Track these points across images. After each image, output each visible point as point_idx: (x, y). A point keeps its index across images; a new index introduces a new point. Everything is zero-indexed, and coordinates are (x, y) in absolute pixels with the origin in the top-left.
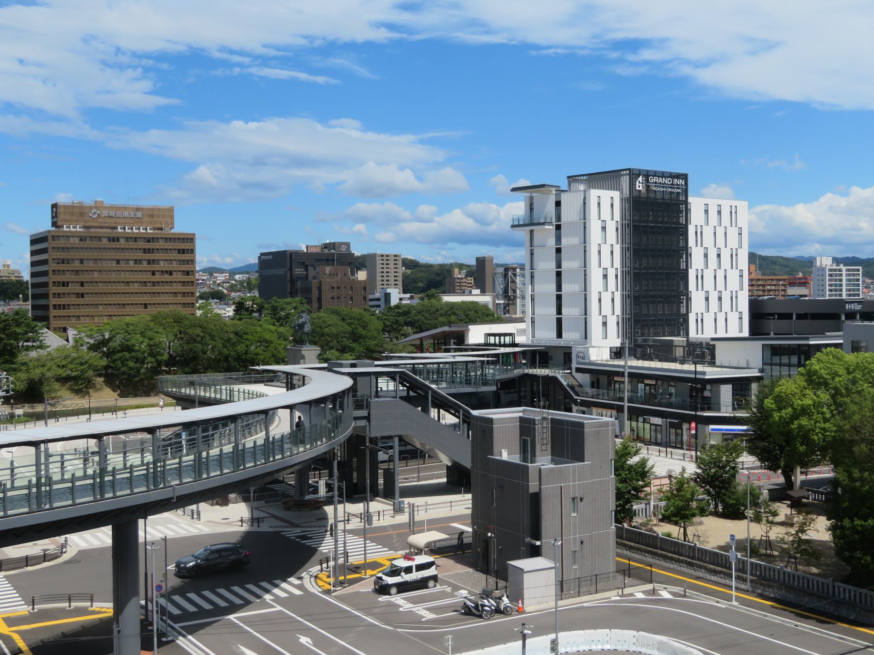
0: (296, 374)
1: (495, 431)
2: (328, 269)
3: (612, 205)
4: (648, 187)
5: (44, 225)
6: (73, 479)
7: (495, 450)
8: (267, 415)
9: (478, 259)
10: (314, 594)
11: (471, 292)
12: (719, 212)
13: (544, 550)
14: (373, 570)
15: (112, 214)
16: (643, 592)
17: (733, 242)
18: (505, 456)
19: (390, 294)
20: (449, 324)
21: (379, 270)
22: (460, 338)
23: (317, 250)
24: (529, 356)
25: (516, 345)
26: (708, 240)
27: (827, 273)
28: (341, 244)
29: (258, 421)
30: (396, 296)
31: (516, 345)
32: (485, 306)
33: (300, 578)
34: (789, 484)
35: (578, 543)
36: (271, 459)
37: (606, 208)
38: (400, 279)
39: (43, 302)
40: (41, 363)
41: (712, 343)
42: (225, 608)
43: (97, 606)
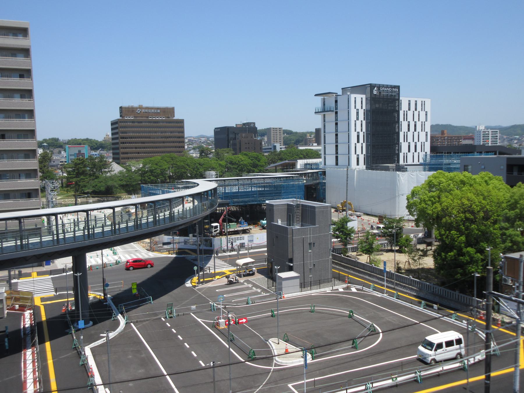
1: (275, 210)
2: (244, 135)
3: (362, 102)
5: (117, 116)
7: (275, 219)
12: (416, 104)
13: (294, 268)
15: (146, 111)
17: (423, 118)
18: (280, 223)
22: (293, 165)
23: (241, 126)
26: (410, 118)
27: (482, 133)
28: (251, 123)
37: (358, 103)
39: (117, 151)
40: (112, 178)
41: (405, 167)
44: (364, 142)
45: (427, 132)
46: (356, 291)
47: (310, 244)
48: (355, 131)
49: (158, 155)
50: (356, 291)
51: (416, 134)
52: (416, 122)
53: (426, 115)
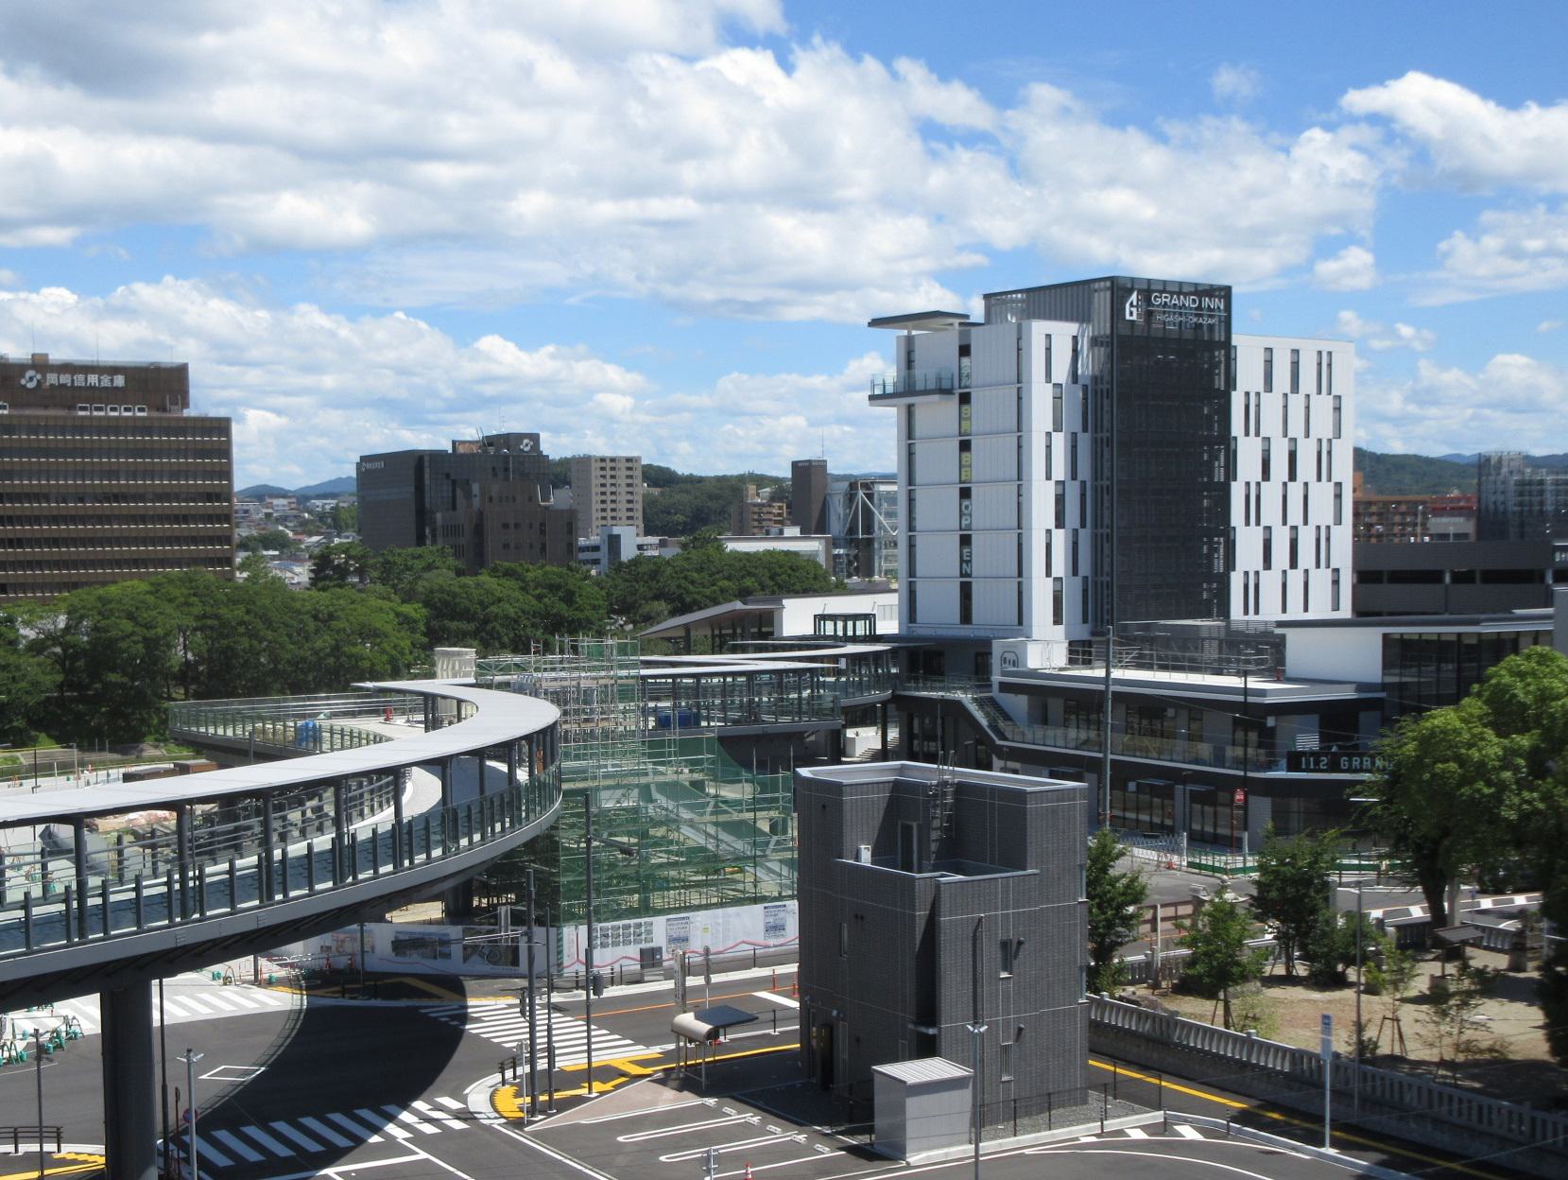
0: (444, 697)
1: (847, 808)
6: (26, 904)
8: (392, 778)
9: (796, 466)
11: (781, 532)
12: (1295, 366)
13: (944, 1044)
14: (604, 1082)
15: (66, 379)
16: (1144, 1128)
17: (1322, 427)
19: (618, 537)
20: (744, 594)
21: (596, 489)
22: (761, 631)
28: (521, 436)
29: (380, 788)
30: (632, 541)
32: (811, 558)
34: (1439, 918)
35: (1013, 1032)
36: (407, 863)
41: (1279, 631)
42: (286, 1159)
43: (68, 1150)
44: (1083, 525)
45: (1339, 485)
46: (1197, 1136)
47: (1005, 945)
48: (1049, 477)
49: (132, 576)
50: (1197, 1136)
51: (1295, 491)
52: (1294, 440)
53: (1338, 409)
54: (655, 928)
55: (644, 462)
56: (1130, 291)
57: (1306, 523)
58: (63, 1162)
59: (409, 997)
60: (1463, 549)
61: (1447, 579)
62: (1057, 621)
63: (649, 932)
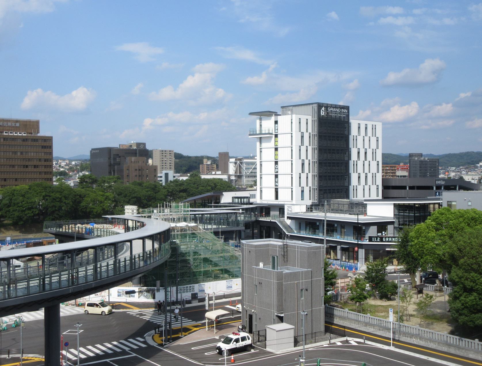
2: (133, 159)
4: (328, 113)
10: (153, 347)
12: (366, 128)
16: (341, 342)
17: (374, 145)
22: (216, 201)
24: (259, 210)
25: (252, 204)
31: (252, 204)
33: (144, 338)
38: (173, 165)
41: (365, 202)
44: (309, 172)
51: (366, 163)
53: (377, 141)
54: (195, 287)
55: (175, 152)
56: (322, 107)
57: (369, 172)
58: (24, 360)
59: (123, 309)
60: (415, 180)
61: (408, 189)
62: (310, 199)
63: (193, 289)
